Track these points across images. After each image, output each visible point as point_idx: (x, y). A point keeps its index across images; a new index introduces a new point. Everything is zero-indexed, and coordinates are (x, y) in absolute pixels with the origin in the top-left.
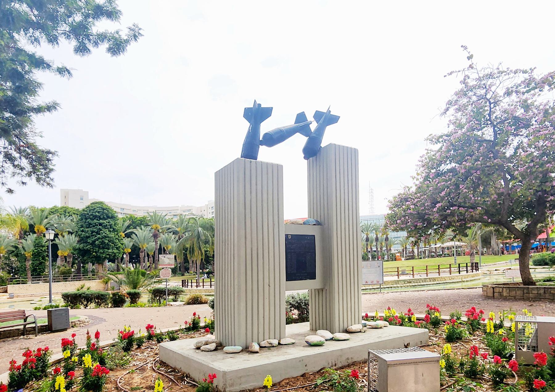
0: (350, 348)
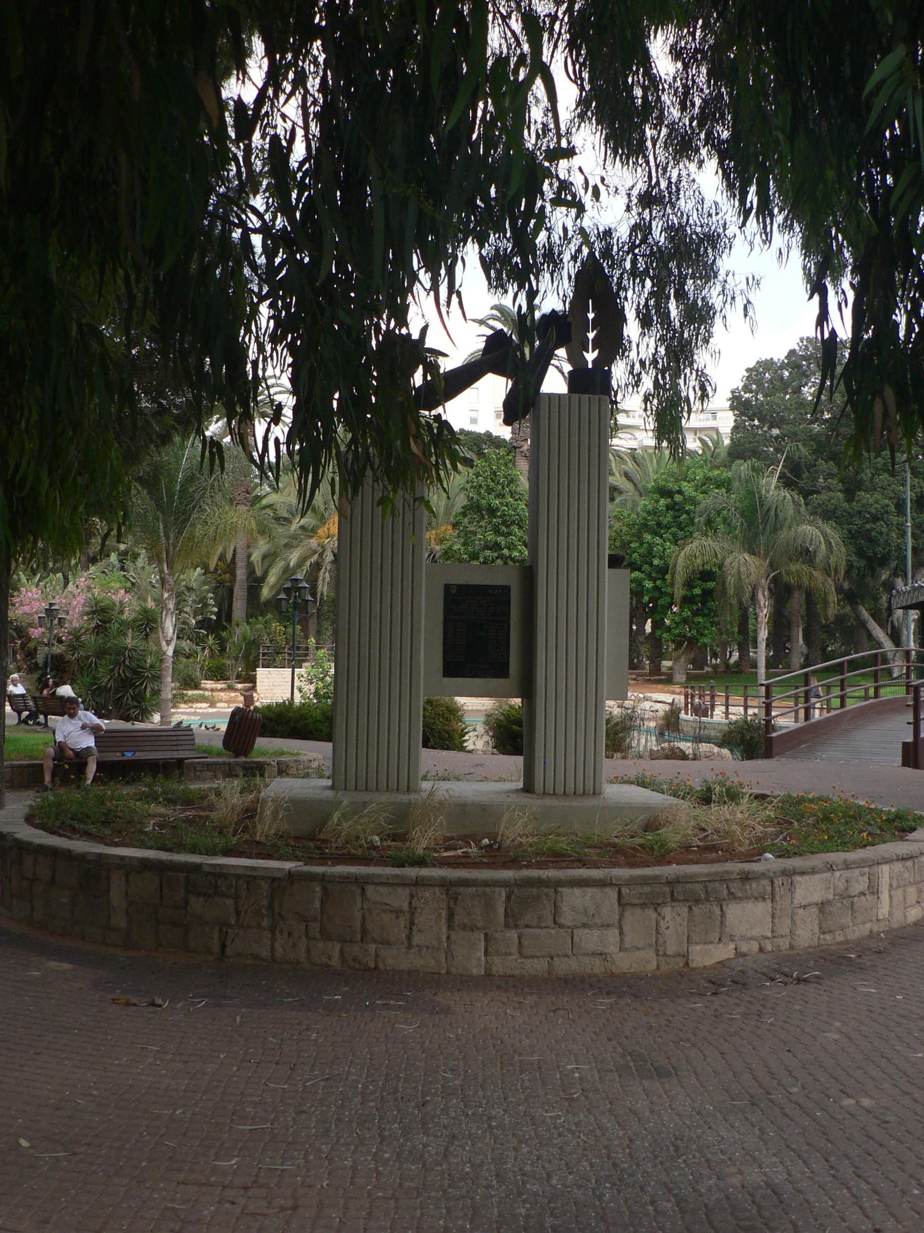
0: (192, 863)
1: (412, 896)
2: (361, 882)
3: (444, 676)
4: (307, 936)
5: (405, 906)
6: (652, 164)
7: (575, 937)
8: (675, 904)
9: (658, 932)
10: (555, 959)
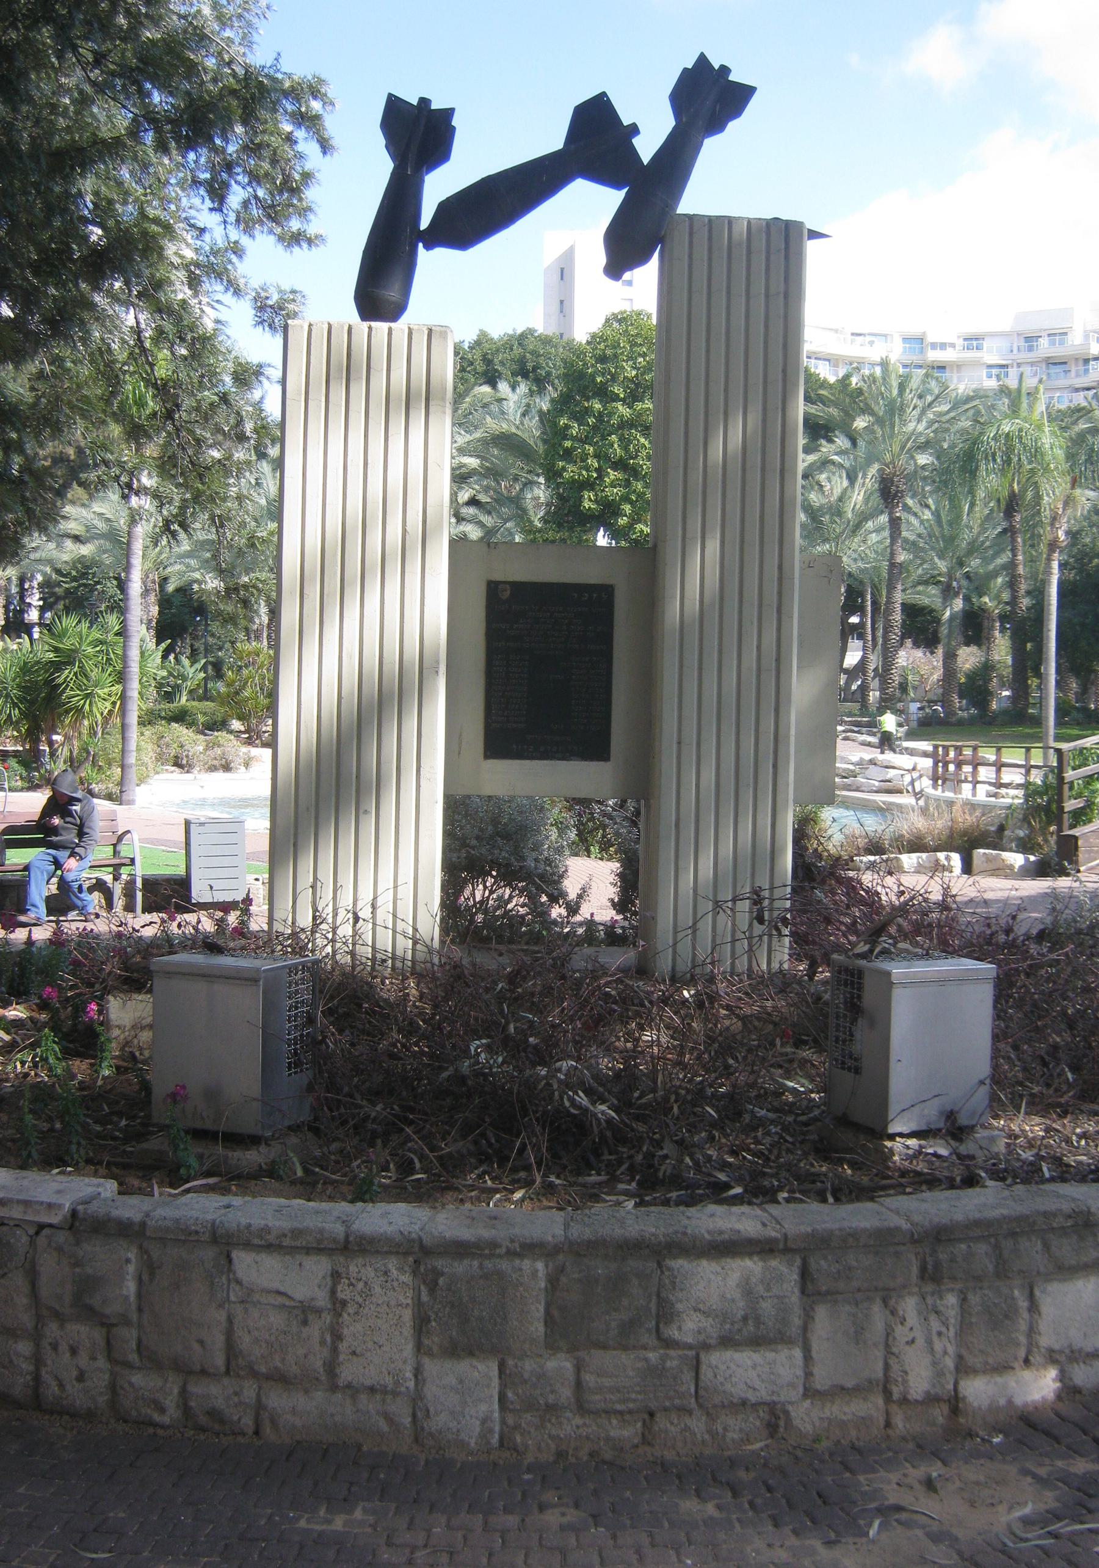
1: (336, 1276)
2: (224, 1242)
3: (487, 756)
4: (110, 1358)
5: (322, 1299)
6: (952, 414)
7: (703, 1368)
8: (763, 1394)
9: (889, 1352)
10: (658, 1417)
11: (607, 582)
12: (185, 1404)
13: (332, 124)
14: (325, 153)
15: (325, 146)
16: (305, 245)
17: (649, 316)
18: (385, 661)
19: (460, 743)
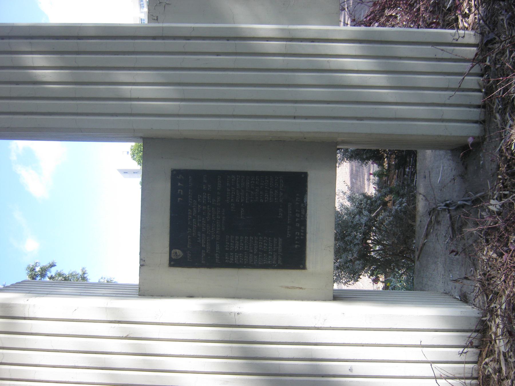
3: (304, 268)
11: (169, 174)
12: (454, 281)
13: (45, 263)
14: (55, 265)
15: (52, 265)
16: (85, 276)
17: (132, 146)
18: (230, 355)
19: (293, 288)
